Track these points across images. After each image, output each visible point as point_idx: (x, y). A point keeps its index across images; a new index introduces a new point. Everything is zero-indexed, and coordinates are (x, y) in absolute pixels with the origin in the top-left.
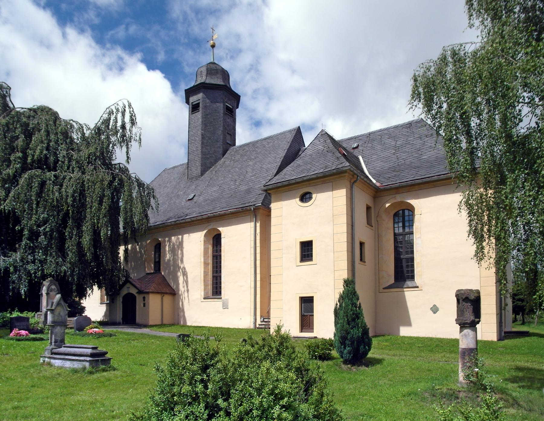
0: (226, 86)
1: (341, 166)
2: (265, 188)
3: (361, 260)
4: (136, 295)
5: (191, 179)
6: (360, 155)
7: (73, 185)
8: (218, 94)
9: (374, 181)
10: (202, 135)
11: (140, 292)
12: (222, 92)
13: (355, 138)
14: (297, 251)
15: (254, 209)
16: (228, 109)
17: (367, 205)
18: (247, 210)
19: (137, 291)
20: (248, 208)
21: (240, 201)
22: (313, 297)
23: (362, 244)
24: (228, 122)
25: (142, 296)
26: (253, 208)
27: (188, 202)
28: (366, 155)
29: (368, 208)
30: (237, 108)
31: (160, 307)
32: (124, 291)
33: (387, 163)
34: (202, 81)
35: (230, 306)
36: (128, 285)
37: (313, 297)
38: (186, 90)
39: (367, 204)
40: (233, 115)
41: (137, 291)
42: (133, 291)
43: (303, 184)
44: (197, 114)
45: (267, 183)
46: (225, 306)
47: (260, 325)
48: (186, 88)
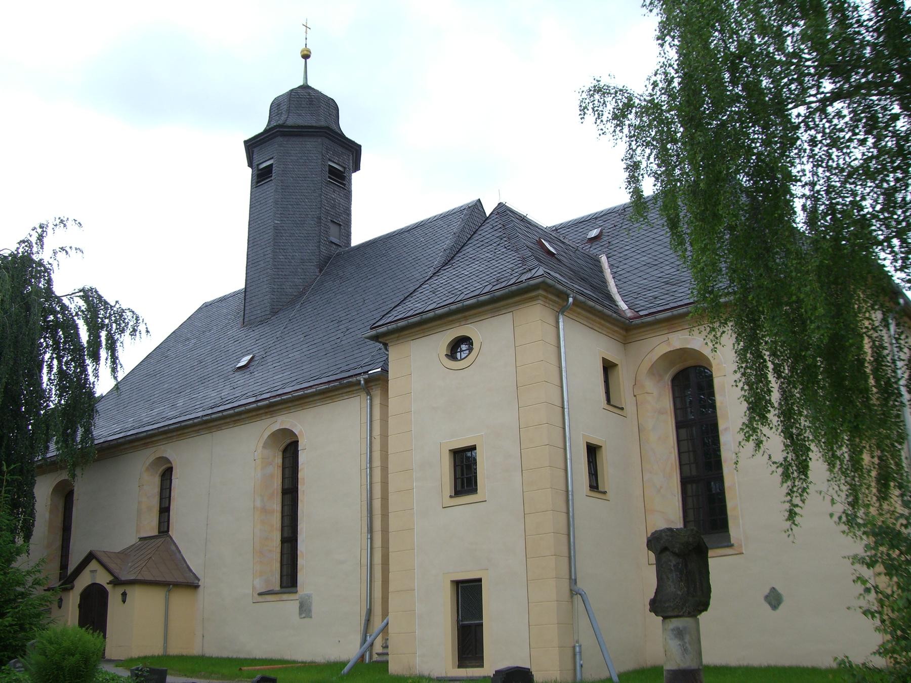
0: (328, 128)
1: (529, 275)
2: (373, 332)
3: (594, 486)
4: (109, 588)
5: (248, 321)
6: (603, 253)
7: (10, 345)
8: (312, 146)
9: (623, 306)
10: (276, 228)
11: (117, 582)
12: (320, 140)
13: (596, 218)
14: (445, 470)
15: (366, 381)
16: (333, 171)
17: (605, 361)
18: (351, 385)
19: (110, 578)
20: (354, 379)
21: (339, 366)
22: (480, 580)
23: (592, 451)
24: (334, 200)
25: (120, 590)
26: (365, 379)
27: (237, 374)
28: (616, 253)
29: (608, 367)
30: (357, 168)
31: (735, 556)
32: (83, 581)
33: (656, 267)
34: (280, 122)
35: (315, 609)
36: (94, 565)
37: (480, 580)
38: (246, 142)
39: (604, 359)
40: (344, 185)
41: (110, 578)
42: (103, 578)
43: (450, 318)
44: (265, 187)
45: (374, 324)
46: (305, 609)
47: (378, 654)
48: (247, 138)
